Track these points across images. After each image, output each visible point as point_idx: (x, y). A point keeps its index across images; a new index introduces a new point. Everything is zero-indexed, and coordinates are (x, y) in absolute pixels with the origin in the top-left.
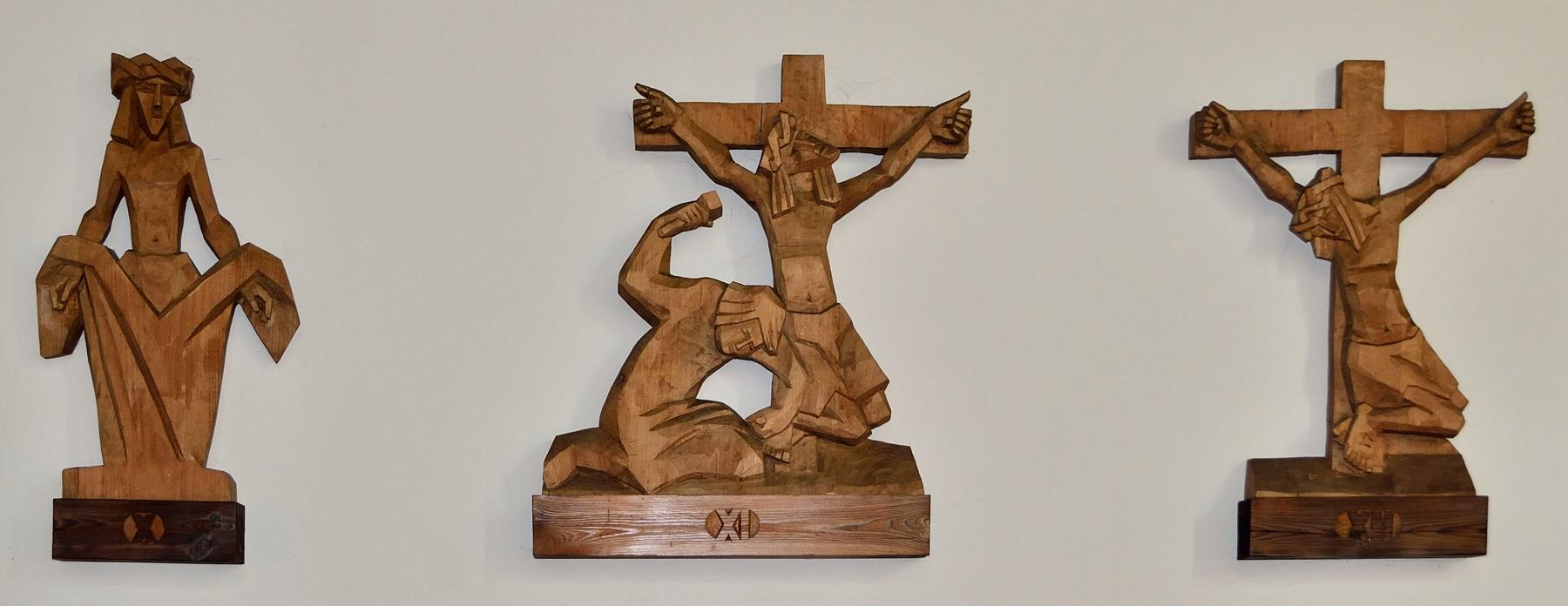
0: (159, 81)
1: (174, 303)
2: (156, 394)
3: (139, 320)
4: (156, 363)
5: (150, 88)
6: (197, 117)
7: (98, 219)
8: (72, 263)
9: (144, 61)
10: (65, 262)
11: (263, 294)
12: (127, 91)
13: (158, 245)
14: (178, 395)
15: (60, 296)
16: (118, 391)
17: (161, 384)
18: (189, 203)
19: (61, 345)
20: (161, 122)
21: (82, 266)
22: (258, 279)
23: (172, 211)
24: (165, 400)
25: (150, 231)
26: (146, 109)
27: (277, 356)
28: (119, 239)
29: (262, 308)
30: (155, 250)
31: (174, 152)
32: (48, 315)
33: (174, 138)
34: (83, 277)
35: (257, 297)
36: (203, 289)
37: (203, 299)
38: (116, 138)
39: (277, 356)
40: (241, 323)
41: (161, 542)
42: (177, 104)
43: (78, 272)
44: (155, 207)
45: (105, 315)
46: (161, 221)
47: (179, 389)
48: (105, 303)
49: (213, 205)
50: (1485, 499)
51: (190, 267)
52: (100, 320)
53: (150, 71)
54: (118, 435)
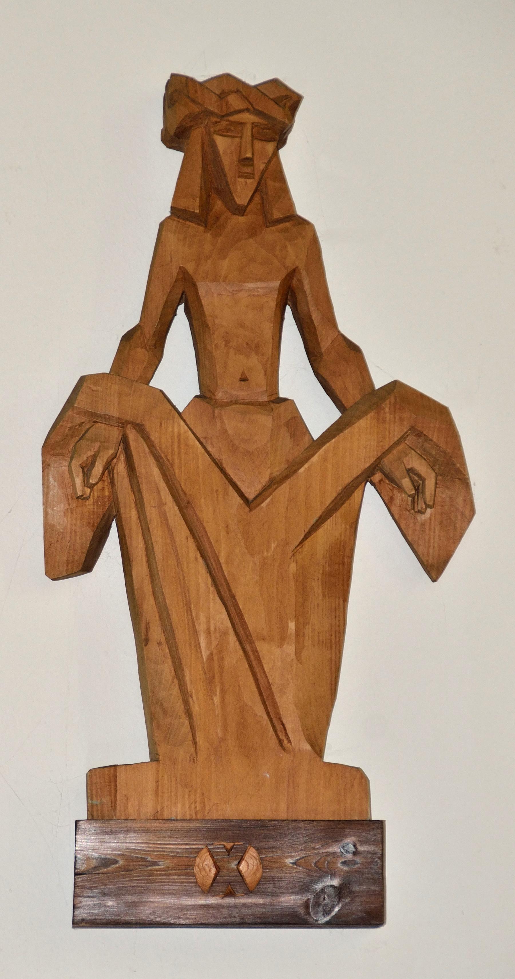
0: (249, 118)
1: (274, 483)
2: (244, 637)
3: (218, 513)
4: (245, 588)
5: (233, 130)
6: (305, 166)
7: (143, 345)
8: (106, 419)
9: (228, 85)
10: (95, 417)
11: (421, 467)
12: (197, 134)
13: (237, 385)
14: (283, 638)
15: (86, 475)
16: (182, 636)
17: (255, 620)
18: (288, 309)
19: (80, 556)
20: (252, 183)
21: (123, 424)
22: (410, 440)
23: (268, 329)
24: (262, 647)
25: (233, 364)
26: (228, 162)
27: (434, 568)
28: (177, 375)
29: (419, 489)
30: (243, 395)
31: (270, 235)
32: (60, 507)
33: (272, 209)
34: (125, 440)
35: (410, 471)
36: (324, 460)
37: (318, 481)
38: (176, 211)
39: (434, 568)
40: (371, 501)
41: (209, 891)
42: (275, 154)
43: (115, 434)
44: (242, 326)
45: (161, 504)
46: (252, 347)
47: (283, 630)
48: (163, 485)
49: (330, 320)
50: (380, 824)
51: (295, 423)
52: (152, 513)
53: (235, 102)
54: (179, 707)
